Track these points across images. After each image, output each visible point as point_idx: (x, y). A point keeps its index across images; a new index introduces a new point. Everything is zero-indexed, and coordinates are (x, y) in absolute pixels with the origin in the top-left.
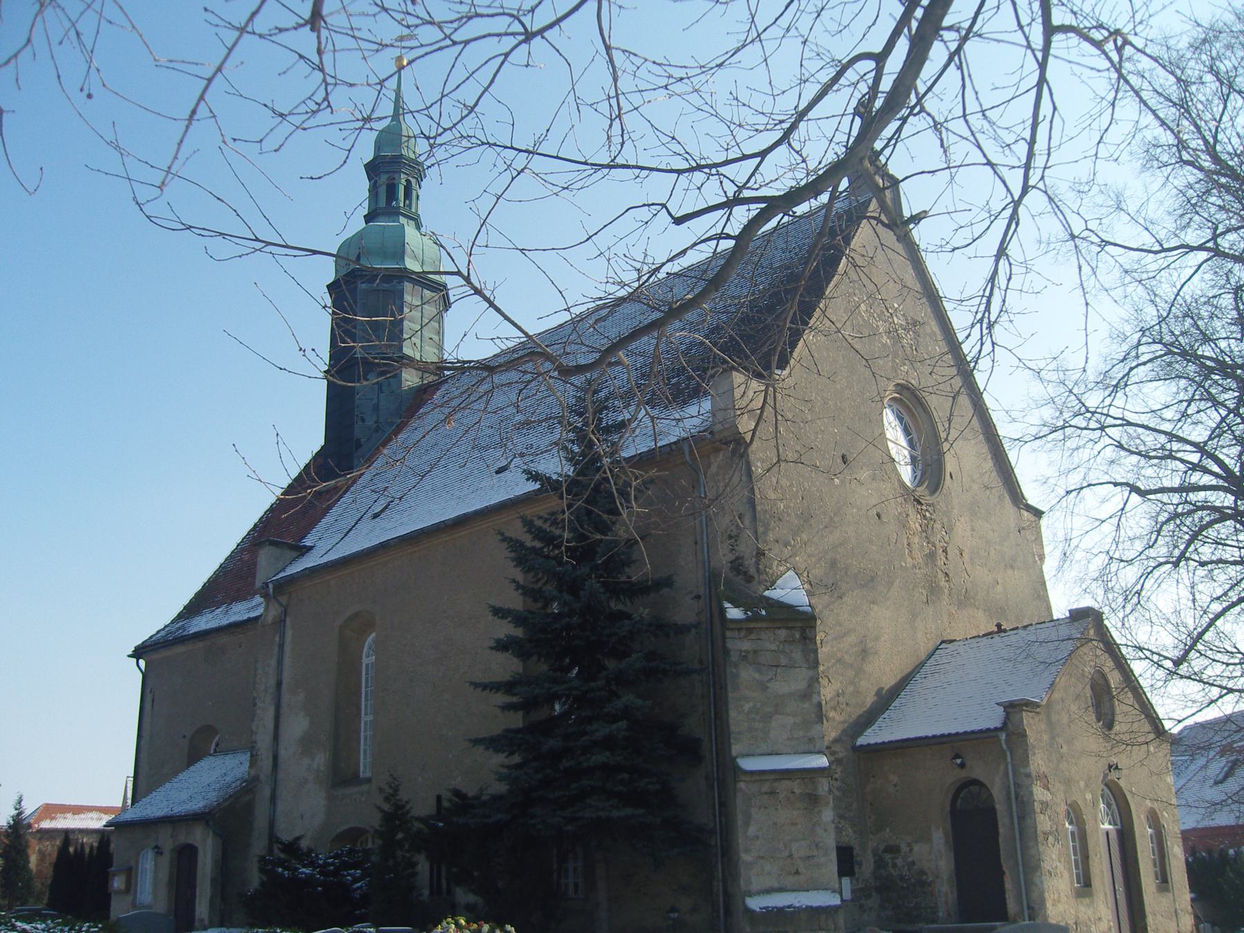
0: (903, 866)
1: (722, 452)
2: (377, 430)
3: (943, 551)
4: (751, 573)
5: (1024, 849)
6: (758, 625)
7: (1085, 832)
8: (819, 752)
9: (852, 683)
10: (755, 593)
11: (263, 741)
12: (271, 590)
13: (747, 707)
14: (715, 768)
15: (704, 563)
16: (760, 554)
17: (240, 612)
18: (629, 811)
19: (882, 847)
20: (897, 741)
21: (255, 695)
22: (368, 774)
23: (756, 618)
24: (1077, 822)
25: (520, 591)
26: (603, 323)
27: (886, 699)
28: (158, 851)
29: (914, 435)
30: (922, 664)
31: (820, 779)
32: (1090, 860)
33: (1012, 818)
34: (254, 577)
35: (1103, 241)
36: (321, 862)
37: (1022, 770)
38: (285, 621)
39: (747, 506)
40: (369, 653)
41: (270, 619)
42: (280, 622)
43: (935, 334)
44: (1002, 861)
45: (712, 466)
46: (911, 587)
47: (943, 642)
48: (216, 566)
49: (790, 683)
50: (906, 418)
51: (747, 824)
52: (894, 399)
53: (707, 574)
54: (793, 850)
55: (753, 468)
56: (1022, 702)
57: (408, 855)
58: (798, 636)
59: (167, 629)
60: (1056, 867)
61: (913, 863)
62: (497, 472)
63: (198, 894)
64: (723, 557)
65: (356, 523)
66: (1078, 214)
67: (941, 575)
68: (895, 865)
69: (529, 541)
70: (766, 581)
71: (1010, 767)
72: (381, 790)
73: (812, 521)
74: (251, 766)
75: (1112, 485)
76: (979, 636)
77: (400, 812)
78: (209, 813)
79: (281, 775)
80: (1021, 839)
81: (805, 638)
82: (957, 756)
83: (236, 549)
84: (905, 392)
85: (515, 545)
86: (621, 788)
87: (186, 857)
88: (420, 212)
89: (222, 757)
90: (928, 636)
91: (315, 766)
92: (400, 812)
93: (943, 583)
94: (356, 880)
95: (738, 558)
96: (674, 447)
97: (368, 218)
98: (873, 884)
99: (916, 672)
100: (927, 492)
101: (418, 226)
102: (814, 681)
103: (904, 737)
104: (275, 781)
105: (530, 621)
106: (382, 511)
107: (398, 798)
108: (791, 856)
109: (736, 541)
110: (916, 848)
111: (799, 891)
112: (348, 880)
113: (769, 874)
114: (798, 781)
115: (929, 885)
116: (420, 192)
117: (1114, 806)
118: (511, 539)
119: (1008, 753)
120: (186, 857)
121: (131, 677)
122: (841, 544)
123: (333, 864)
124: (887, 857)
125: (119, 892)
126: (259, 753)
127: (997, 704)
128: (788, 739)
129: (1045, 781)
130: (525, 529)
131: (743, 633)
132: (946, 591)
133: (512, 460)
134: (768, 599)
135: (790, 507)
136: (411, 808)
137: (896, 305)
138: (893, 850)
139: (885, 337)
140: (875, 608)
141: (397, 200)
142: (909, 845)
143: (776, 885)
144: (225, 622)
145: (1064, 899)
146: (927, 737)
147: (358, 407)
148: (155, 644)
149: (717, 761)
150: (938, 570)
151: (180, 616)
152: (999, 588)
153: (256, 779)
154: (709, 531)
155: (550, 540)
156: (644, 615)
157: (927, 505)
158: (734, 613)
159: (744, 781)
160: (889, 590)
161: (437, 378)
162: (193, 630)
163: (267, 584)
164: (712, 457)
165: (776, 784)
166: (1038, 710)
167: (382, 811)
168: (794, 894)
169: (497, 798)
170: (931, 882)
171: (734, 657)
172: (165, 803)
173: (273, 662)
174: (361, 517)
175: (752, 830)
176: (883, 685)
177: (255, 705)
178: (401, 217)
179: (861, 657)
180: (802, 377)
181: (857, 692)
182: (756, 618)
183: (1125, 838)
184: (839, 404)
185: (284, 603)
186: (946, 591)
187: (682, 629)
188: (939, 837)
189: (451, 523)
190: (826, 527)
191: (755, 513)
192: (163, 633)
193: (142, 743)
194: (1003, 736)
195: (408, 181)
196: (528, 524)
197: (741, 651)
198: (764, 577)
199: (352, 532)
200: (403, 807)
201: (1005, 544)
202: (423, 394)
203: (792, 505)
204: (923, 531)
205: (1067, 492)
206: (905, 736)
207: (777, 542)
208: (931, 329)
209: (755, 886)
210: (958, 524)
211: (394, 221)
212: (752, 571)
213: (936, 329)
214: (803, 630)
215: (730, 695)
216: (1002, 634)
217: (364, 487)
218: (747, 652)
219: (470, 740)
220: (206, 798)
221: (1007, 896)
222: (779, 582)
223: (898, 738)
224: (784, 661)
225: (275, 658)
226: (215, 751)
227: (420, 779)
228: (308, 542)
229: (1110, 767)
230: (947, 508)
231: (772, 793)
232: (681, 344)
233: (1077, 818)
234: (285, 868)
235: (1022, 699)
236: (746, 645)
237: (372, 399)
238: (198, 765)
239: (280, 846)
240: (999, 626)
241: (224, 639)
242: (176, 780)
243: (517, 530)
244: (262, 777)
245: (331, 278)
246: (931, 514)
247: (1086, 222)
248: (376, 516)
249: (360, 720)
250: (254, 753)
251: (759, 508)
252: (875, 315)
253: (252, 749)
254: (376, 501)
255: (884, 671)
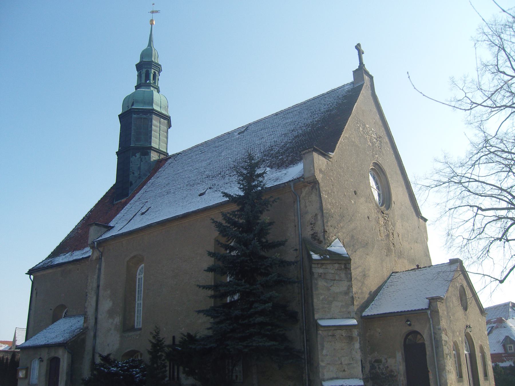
0: (383, 369)
1: (307, 187)
2: (140, 178)
3: (392, 234)
4: (321, 240)
5: (438, 361)
6: (326, 262)
7: (460, 354)
8: (353, 318)
9: (360, 289)
10: (323, 248)
11: (91, 311)
12: (96, 245)
13: (321, 298)
14: (304, 325)
15: (299, 235)
16: (325, 231)
17: (78, 255)
18: (272, 343)
19: (373, 360)
20: (381, 314)
21: (87, 291)
22: (140, 326)
23: (325, 259)
24: (456, 350)
25: (220, 245)
26: (243, 134)
27: (373, 296)
28: (41, 360)
29: (379, 185)
30: (385, 282)
31: (354, 329)
32: (462, 366)
33: (432, 348)
34: (87, 239)
35: (472, 102)
36: (120, 365)
37: (437, 327)
38: (101, 259)
39: (319, 210)
40: (140, 273)
41: (94, 258)
42: (99, 259)
43: (387, 143)
44: (428, 366)
45: (303, 193)
46: (381, 249)
47: (393, 273)
48: (66, 235)
49: (340, 288)
50: (376, 177)
51: (322, 349)
52: (372, 169)
53: (301, 240)
54: (342, 361)
55: (322, 194)
56: (437, 297)
57: (163, 362)
58: (343, 267)
59: (44, 262)
60: (451, 369)
61: (388, 367)
62: (200, 195)
63: (60, 379)
64: (308, 233)
65: (134, 217)
66: (463, 90)
67: (391, 244)
68: (379, 368)
69: (224, 222)
70: (328, 243)
71: (432, 325)
72: (151, 333)
73: (344, 218)
74: (85, 322)
75: (469, 207)
76: (409, 270)
77: (160, 343)
78: (66, 343)
79: (99, 326)
80: (437, 357)
81: (346, 268)
82: (408, 321)
83: (75, 228)
84: (377, 166)
85: (219, 225)
86: (268, 333)
87: (54, 363)
88: (159, 86)
89: (69, 318)
90: (387, 270)
91: (115, 322)
92: (160, 343)
93: (392, 248)
94: (137, 373)
95: (315, 233)
96: (286, 184)
97: (137, 87)
98: (370, 376)
99: (383, 285)
100: (385, 209)
101: (158, 92)
102: (350, 287)
103: (384, 312)
104: (96, 329)
105: (227, 258)
106: (146, 212)
107: (159, 337)
108: (341, 363)
109: (314, 225)
110: (389, 360)
111: (345, 379)
112: (134, 373)
113: (332, 371)
114: (344, 330)
115: (395, 376)
116: (159, 77)
117: (467, 344)
118: (217, 222)
119: (431, 320)
120: (54, 363)
121: (27, 282)
122: (355, 229)
123: (126, 366)
124: (376, 364)
125: (21, 378)
126: (88, 317)
127: (426, 298)
128: (339, 312)
129: (445, 331)
130: (223, 218)
131: (319, 266)
132: (393, 251)
133: (206, 190)
134: (329, 251)
135: (336, 212)
136: (164, 341)
137: (373, 129)
138: (378, 361)
139: (369, 142)
140: (368, 257)
141: (150, 80)
142: (386, 359)
143: (335, 376)
144: (71, 259)
145: (454, 383)
146: (394, 312)
147: (131, 168)
148: (38, 269)
149: (305, 322)
150: (391, 242)
151: (49, 257)
152: (412, 251)
153: (87, 328)
154: (301, 221)
155: (235, 224)
156: (277, 256)
157: (386, 214)
158: (315, 256)
159: (321, 330)
160: (373, 249)
161: (166, 156)
162: (56, 263)
163: (94, 242)
164: (303, 189)
165: (335, 332)
166: (443, 301)
167: (152, 342)
168: (343, 380)
169: (208, 337)
170: (396, 375)
171: (316, 276)
172: (44, 339)
173: (96, 277)
174: (136, 214)
175: (324, 352)
176: (371, 290)
177: (87, 295)
178: (151, 88)
179: (363, 278)
180: (339, 157)
181: (362, 293)
182: (325, 259)
183: (472, 356)
184: (353, 169)
185: (101, 251)
186: (393, 251)
187: (289, 263)
188: (399, 356)
189: (181, 216)
190: (349, 221)
191: (323, 213)
192: (42, 264)
193: (31, 312)
194: (429, 312)
195: (154, 72)
196: (224, 215)
197: (318, 273)
198: (327, 241)
199: (132, 220)
200: (162, 340)
201: (414, 232)
202: (160, 163)
203: (337, 211)
204: (385, 225)
205: (449, 209)
206: (384, 312)
207: (332, 226)
208: (386, 140)
209: (326, 377)
210: (397, 223)
211: (148, 89)
212: (322, 239)
213: (387, 140)
214: (345, 264)
215: (314, 292)
216: (420, 270)
217: (136, 202)
218: (321, 273)
219: (196, 311)
220: (64, 336)
221: (430, 382)
222: (332, 244)
223: (382, 312)
224: (337, 278)
225: (97, 275)
226: (65, 316)
227: (165, 329)
228: (111, 224)
229: (467, 326)
230: (393, 216)
231: (333, 335)
232: (281, 142)
233: (456, 348)
234: (105, 368)
235: (437, 296)
236: (321, 271)
237: (138, 164)
238: (58, 322)
239: (101, 358)
240: (418, 266)
241: (71, 267)
242: (48, 329)
243: (220, 219)
244: (90, 327)
245: (120, 112)
246: (387, 218)
247: (466, 93)
248: (143, 214)
249: (136, 303)
250: (86, 317)
251: (324, 211)
252: (365, 133)
253: (85, 315)
254: (142, 208)
255: (372, 284)
